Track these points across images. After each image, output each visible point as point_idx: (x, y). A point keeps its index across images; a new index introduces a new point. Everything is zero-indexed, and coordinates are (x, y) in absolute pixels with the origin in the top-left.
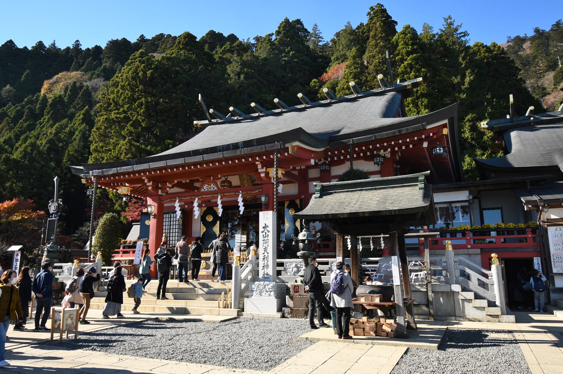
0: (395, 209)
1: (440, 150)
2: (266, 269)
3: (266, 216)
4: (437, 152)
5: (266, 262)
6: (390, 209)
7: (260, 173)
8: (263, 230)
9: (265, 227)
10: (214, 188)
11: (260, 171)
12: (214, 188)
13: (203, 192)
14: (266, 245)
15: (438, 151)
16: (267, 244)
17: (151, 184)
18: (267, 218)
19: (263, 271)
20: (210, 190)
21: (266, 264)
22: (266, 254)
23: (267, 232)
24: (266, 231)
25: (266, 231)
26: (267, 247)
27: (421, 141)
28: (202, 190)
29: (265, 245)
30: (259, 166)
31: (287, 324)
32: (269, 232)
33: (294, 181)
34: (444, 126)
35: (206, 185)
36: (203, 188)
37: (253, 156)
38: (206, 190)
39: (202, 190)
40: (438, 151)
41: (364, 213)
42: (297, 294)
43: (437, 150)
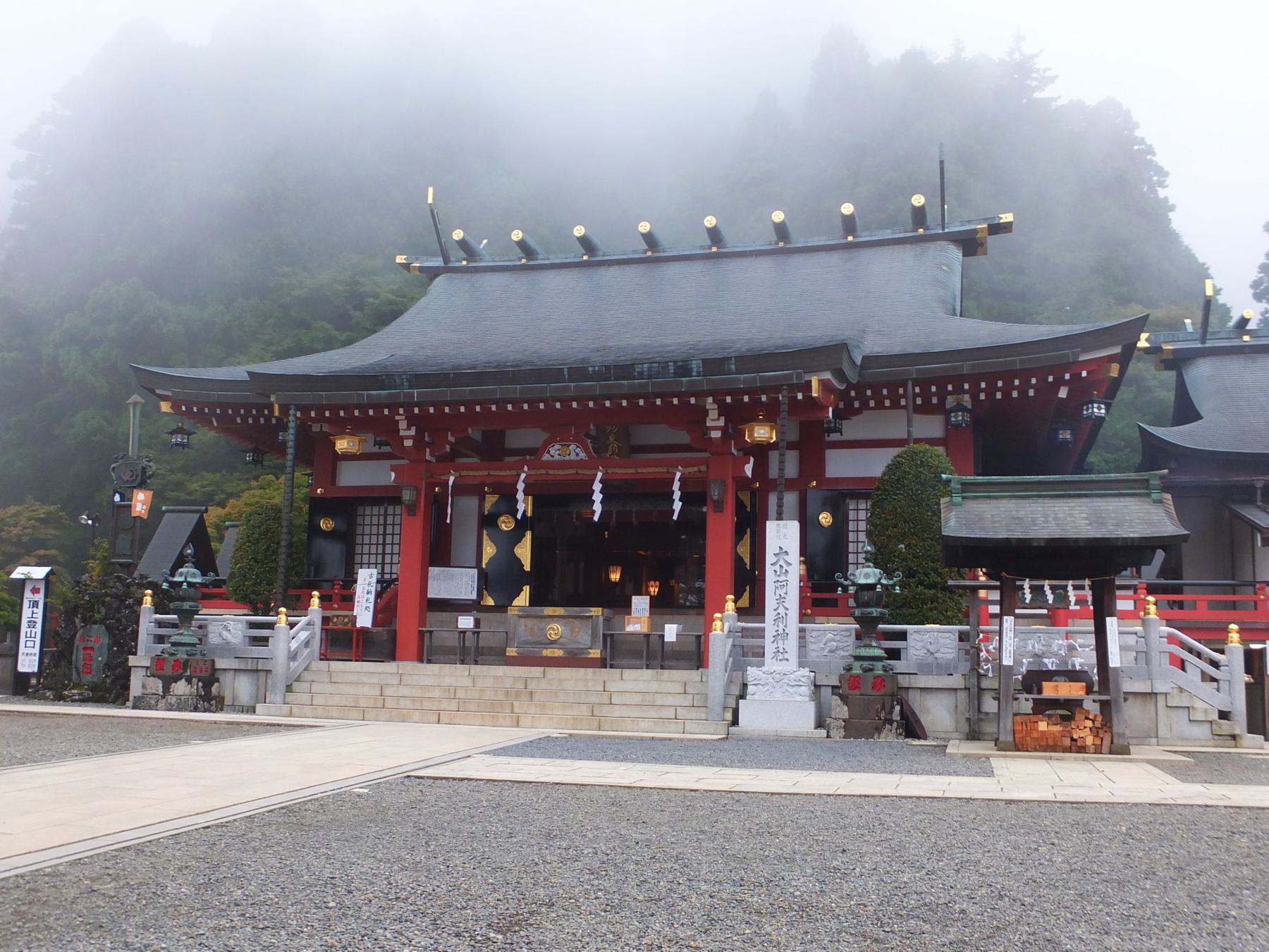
0: (1132, 535)
1: (1099, 408)
2: (780, 642)
3: (783, 531)
4: (1093, 412)
5: (781, 626)
6: (1125, 536)
7: (402, 438)
8: (775, 559)
9: (782, 552)
10: (577, 455)
11: (402, 433)
12: (577, 455)
13: (548, 462)
14: (782, 592)
15: (1096, 410)
16: (784, 590)
17: (413, 432)
18: (785, 535)
19: (775, 645)
20: (567, 458)
21: (781, 631)
22: (781, 610)
23: (784, 565)
24: (781, 562)
25: (781, 562)
26: (783, 595)
27: (1060, 382)
28: (546, 457)
29: (778, 592)
30: (403, 425)
31: (1162, 824)
32: (789, 564)
33: (473, 454)
34: (1111, 359)
35: (557, 446)
36: (548, 452)
37: (394, 407)
38: (557, 457)
39: (546, 457)
40: (1096, 410)
41: (1077, 539)
42: (856, 692)
43: (1093, 407)
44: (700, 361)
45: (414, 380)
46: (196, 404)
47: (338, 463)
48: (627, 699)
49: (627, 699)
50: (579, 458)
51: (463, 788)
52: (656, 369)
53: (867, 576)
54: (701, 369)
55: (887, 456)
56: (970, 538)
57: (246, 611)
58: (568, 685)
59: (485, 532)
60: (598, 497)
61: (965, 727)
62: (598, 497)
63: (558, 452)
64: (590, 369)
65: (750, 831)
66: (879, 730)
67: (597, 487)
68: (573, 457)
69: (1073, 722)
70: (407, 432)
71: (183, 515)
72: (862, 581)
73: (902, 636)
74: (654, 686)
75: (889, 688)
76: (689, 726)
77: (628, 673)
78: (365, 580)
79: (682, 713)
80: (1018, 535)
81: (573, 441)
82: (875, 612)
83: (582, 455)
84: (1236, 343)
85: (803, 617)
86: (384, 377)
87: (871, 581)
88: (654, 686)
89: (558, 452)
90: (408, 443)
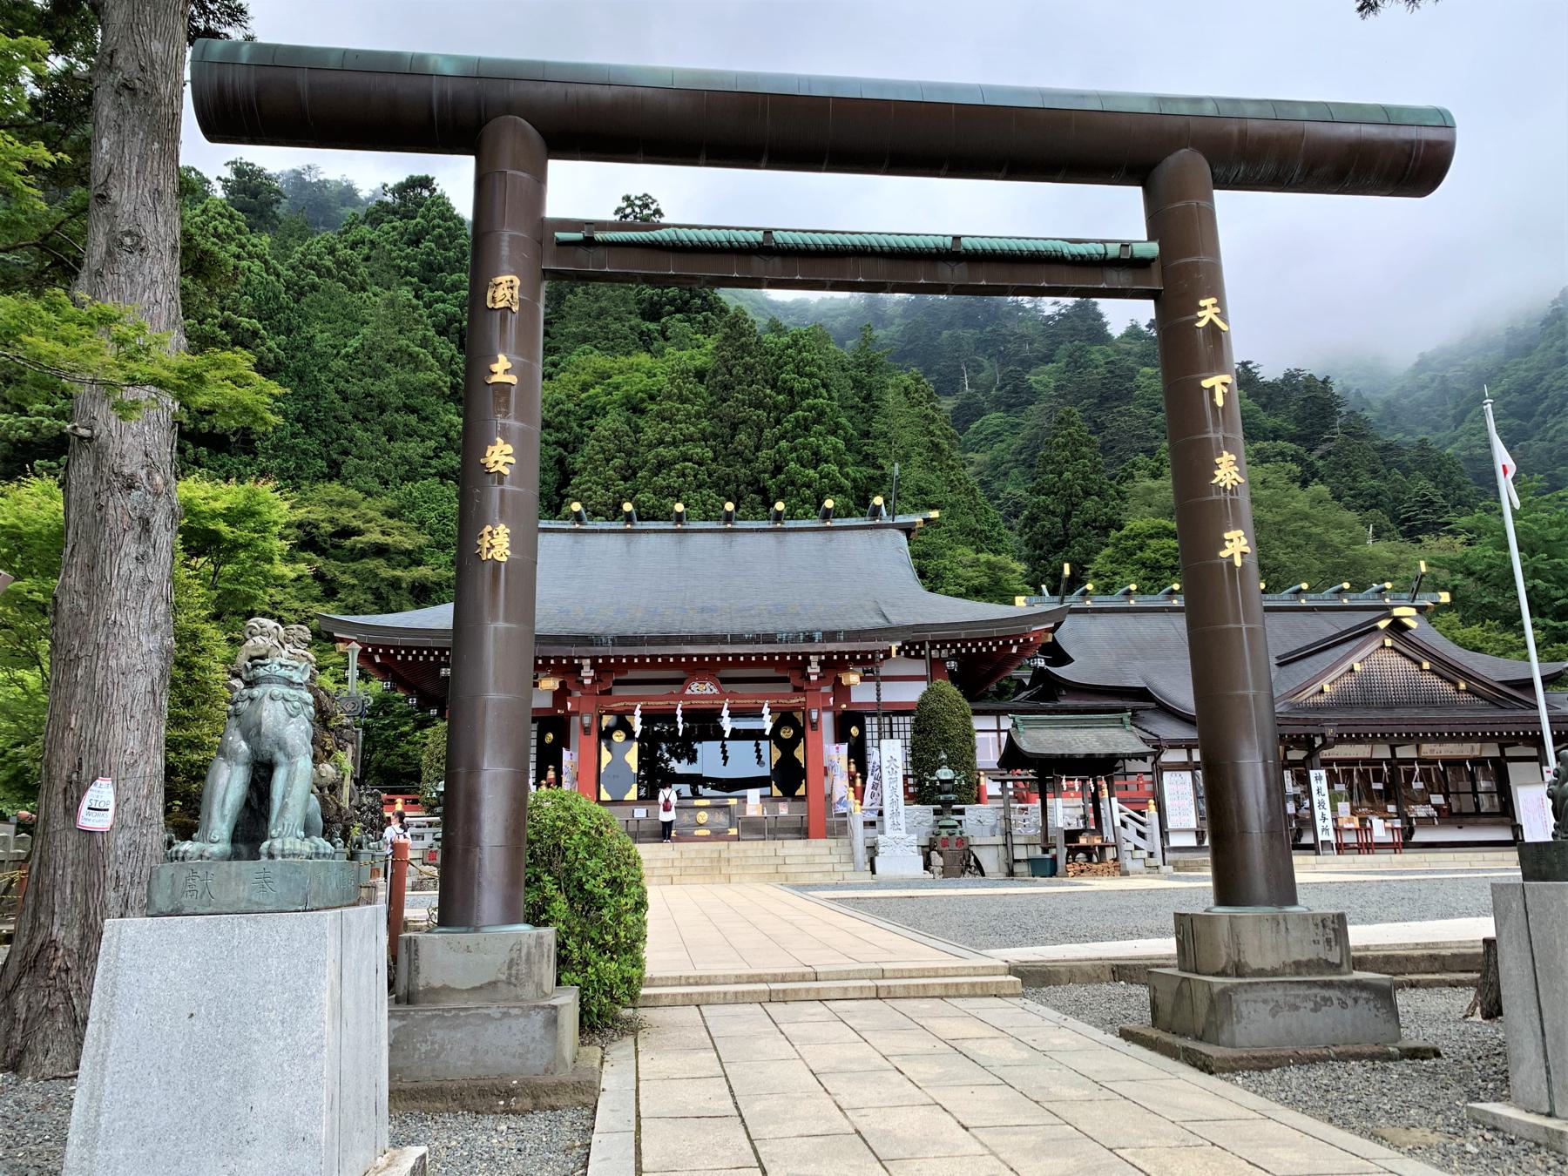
28: (688, 692)
38: (696, 692)
46: (370, 645)
48: (796, 860)
49: (796, 860)
51: (1008, 898)
53: (946, 774)
55: (922, 687)
56: (1535, 880)
57: (420, 814)
58: (750, 853)
59: (603, 744)
60: (680, 719)
61: (1006, 870)
62: (680, 719)
65: (168, 1083)
66: (963, 872)
67: (679, 712)
68: (708, 692)
70: (587, 673)
72: (943, 778)
73: (961, 812)
74: (809, 851)
75: (965, 846)
76: (847, 875)
77: (788, 843)
79: (837, 867)
80: (1067, 752)
82: (953, 797)
83: (715, 691)
84: (1125, 605)
87: (949, 777)
88: (809, 851)
90: (587, 682)
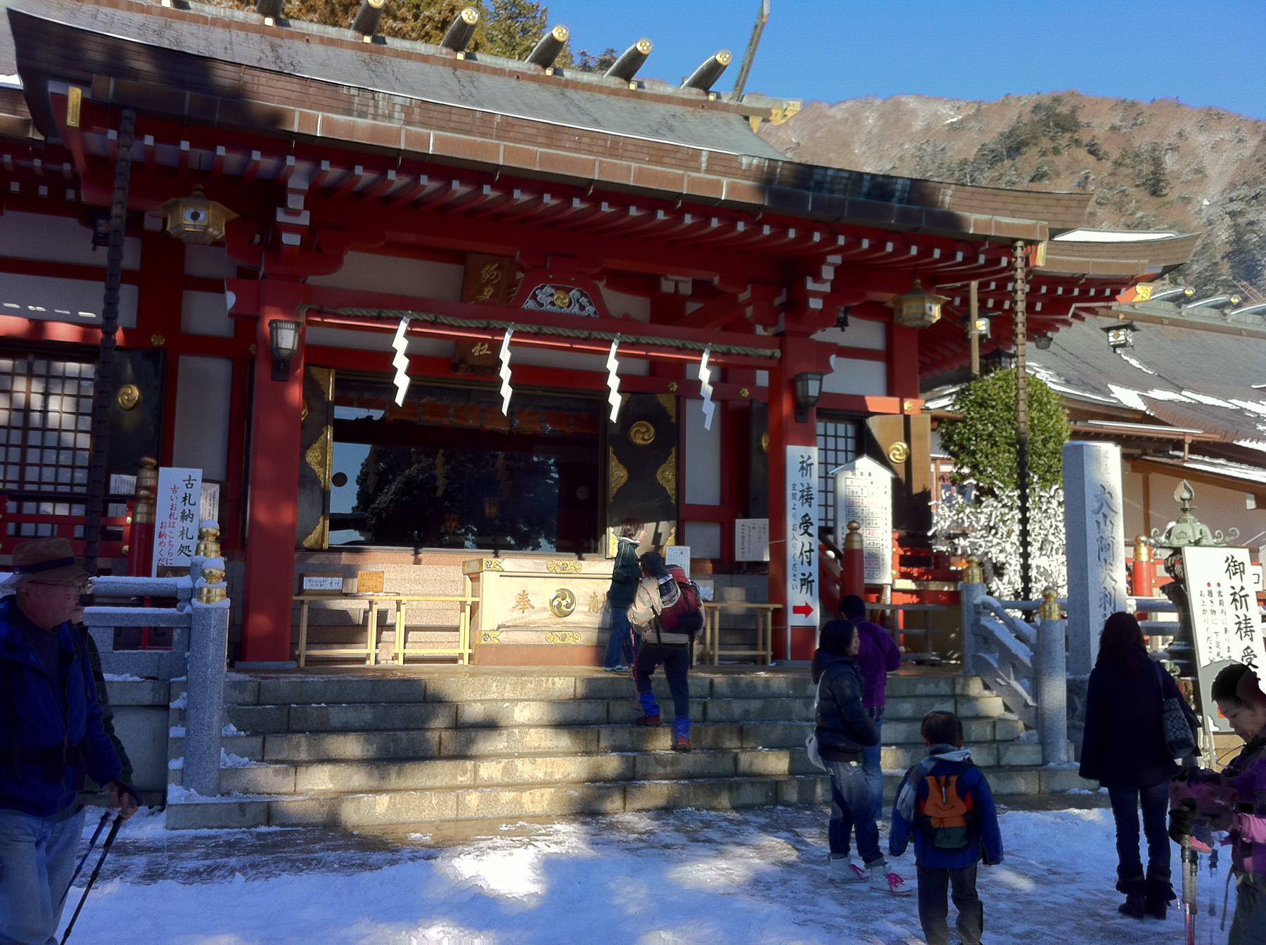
10: (582, 308)
13: (530, 312)
36: (534, 297)
44: (909, 182)
45: (417, 110)
46: (845, 230)
47: (186, 293)
50: (584, 313)
52: (844, 181)
54: (906, 195)
63: (550, 299)
64: (745, 161)
68: (575, 309)
69: (586, 609)
71: (544, 350)
78: (175, 490)
81: (575, 284)
85: (116, 628)
86: (353, 92)
89: (550, 299)
